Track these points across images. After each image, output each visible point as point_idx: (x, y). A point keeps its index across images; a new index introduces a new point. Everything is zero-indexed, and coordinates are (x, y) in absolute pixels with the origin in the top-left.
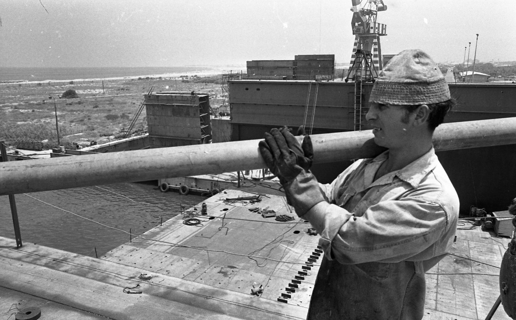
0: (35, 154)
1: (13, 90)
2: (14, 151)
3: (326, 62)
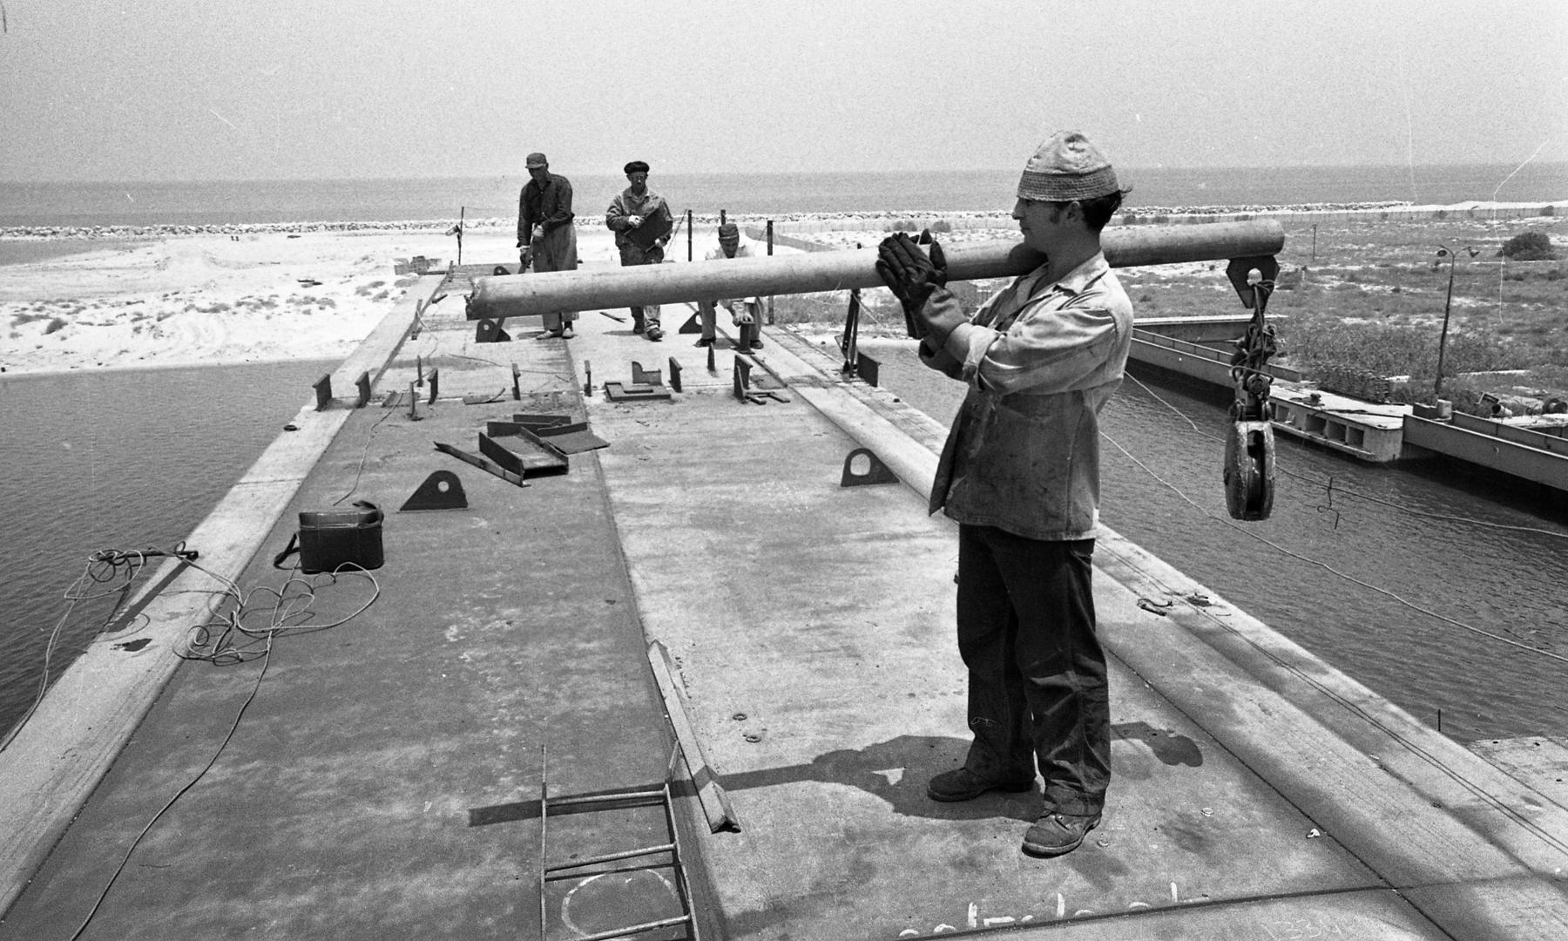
0: (1363, 412)
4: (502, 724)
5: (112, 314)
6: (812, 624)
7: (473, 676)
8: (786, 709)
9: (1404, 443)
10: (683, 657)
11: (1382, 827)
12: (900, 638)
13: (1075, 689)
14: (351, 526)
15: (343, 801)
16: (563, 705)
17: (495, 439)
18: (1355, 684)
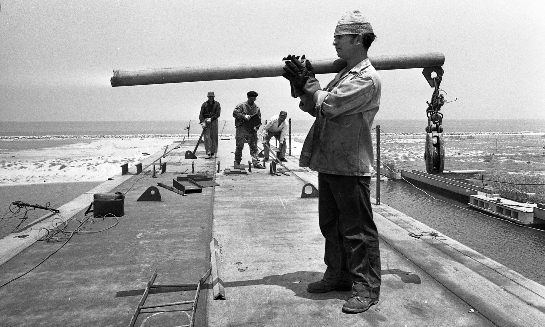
0: (518, 206)
1: (514, 141)
2: (495, 198)
4: (146, 262)
5: (80, 163)
6: (277, 236)
7: (141, 248)
8: (258, 262)
9: (534, 218)
10: (223, 245)
11: (503, 310)
12: (310, 242)
13: (364, 241)
14: (112, 200)
15: (73, 285)
16: (171, 257)
17: (179, 182)
18: (495, 262)
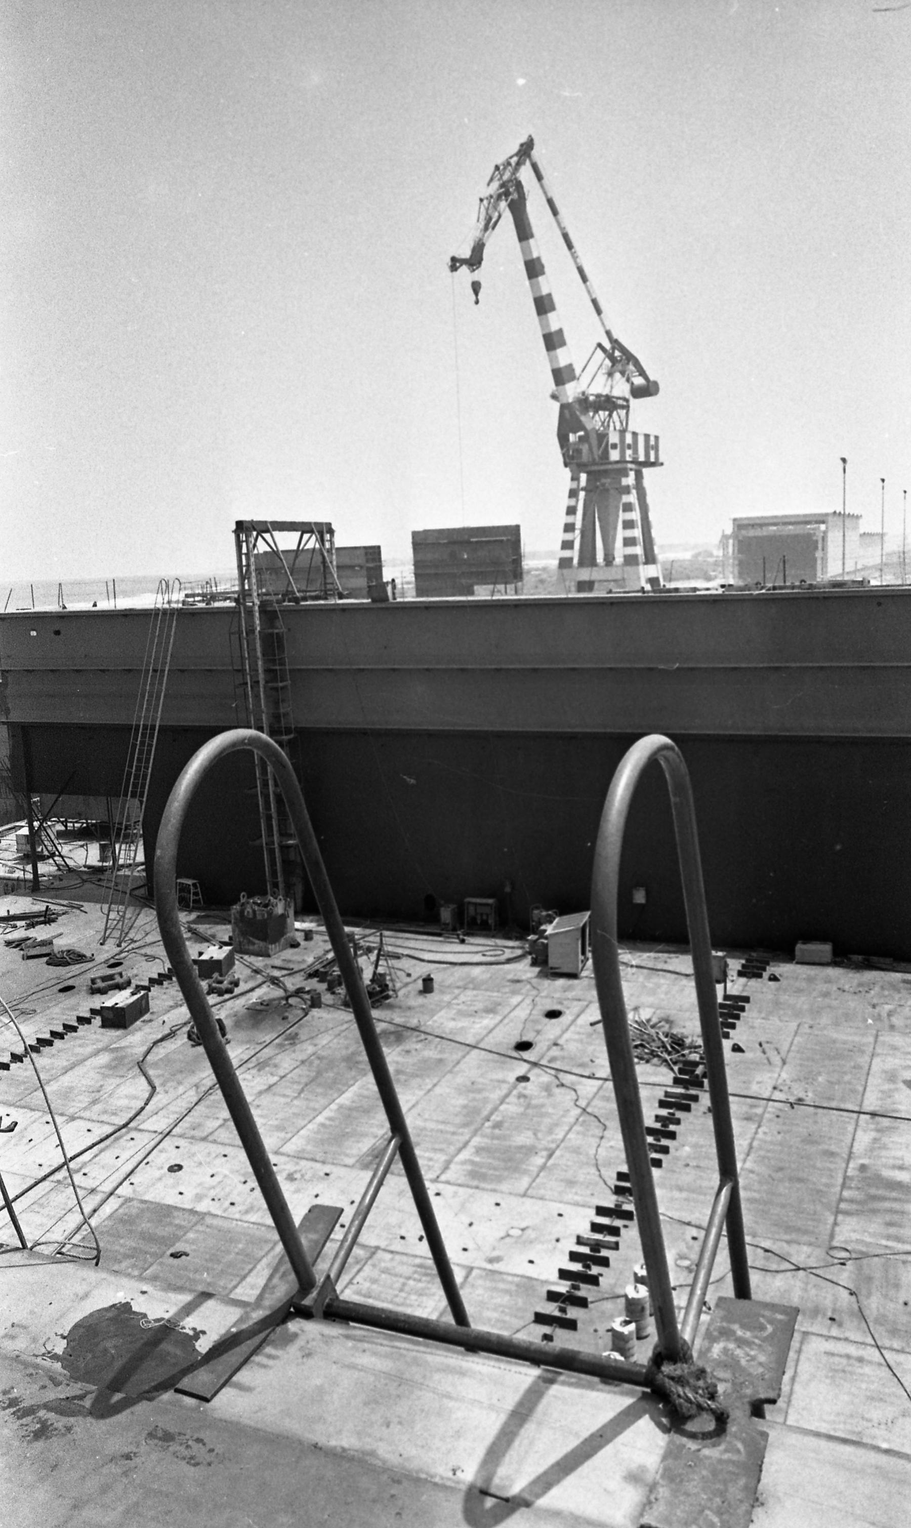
3: (498, 549)
